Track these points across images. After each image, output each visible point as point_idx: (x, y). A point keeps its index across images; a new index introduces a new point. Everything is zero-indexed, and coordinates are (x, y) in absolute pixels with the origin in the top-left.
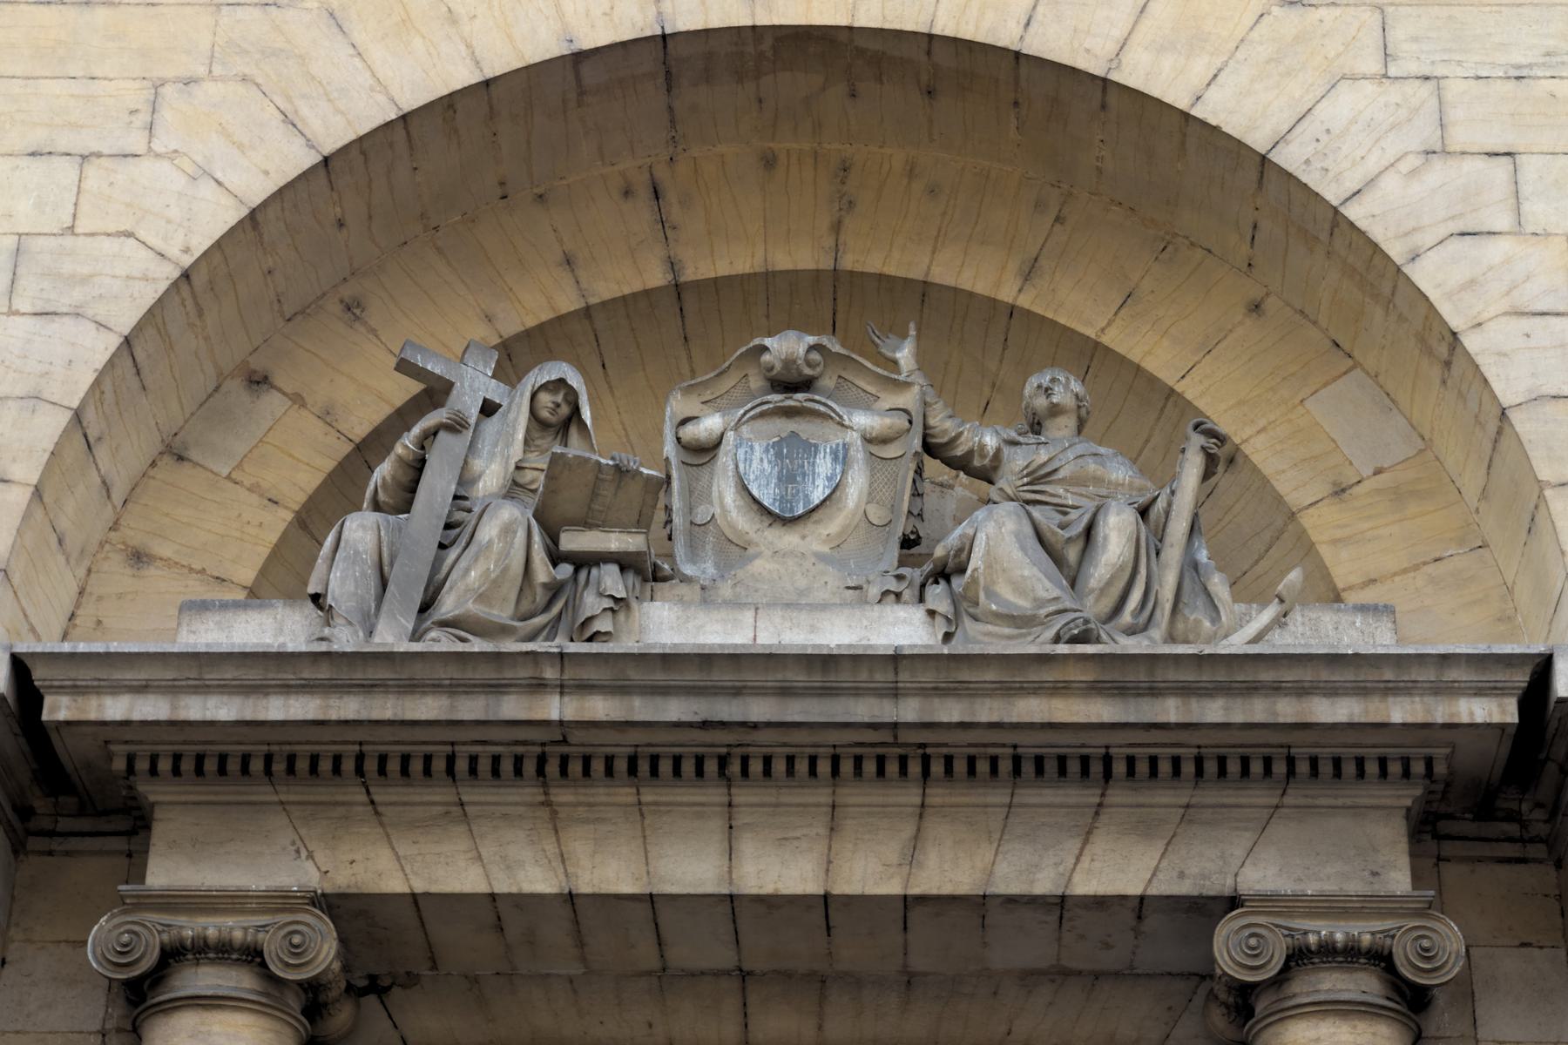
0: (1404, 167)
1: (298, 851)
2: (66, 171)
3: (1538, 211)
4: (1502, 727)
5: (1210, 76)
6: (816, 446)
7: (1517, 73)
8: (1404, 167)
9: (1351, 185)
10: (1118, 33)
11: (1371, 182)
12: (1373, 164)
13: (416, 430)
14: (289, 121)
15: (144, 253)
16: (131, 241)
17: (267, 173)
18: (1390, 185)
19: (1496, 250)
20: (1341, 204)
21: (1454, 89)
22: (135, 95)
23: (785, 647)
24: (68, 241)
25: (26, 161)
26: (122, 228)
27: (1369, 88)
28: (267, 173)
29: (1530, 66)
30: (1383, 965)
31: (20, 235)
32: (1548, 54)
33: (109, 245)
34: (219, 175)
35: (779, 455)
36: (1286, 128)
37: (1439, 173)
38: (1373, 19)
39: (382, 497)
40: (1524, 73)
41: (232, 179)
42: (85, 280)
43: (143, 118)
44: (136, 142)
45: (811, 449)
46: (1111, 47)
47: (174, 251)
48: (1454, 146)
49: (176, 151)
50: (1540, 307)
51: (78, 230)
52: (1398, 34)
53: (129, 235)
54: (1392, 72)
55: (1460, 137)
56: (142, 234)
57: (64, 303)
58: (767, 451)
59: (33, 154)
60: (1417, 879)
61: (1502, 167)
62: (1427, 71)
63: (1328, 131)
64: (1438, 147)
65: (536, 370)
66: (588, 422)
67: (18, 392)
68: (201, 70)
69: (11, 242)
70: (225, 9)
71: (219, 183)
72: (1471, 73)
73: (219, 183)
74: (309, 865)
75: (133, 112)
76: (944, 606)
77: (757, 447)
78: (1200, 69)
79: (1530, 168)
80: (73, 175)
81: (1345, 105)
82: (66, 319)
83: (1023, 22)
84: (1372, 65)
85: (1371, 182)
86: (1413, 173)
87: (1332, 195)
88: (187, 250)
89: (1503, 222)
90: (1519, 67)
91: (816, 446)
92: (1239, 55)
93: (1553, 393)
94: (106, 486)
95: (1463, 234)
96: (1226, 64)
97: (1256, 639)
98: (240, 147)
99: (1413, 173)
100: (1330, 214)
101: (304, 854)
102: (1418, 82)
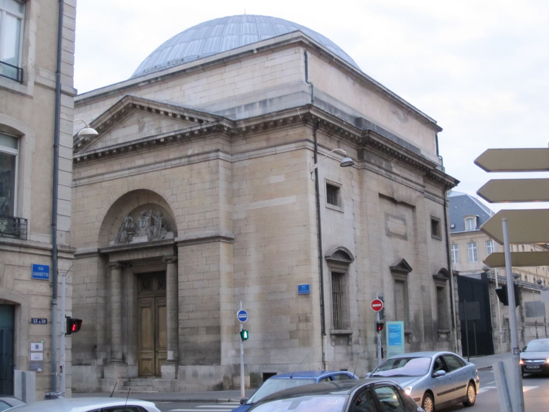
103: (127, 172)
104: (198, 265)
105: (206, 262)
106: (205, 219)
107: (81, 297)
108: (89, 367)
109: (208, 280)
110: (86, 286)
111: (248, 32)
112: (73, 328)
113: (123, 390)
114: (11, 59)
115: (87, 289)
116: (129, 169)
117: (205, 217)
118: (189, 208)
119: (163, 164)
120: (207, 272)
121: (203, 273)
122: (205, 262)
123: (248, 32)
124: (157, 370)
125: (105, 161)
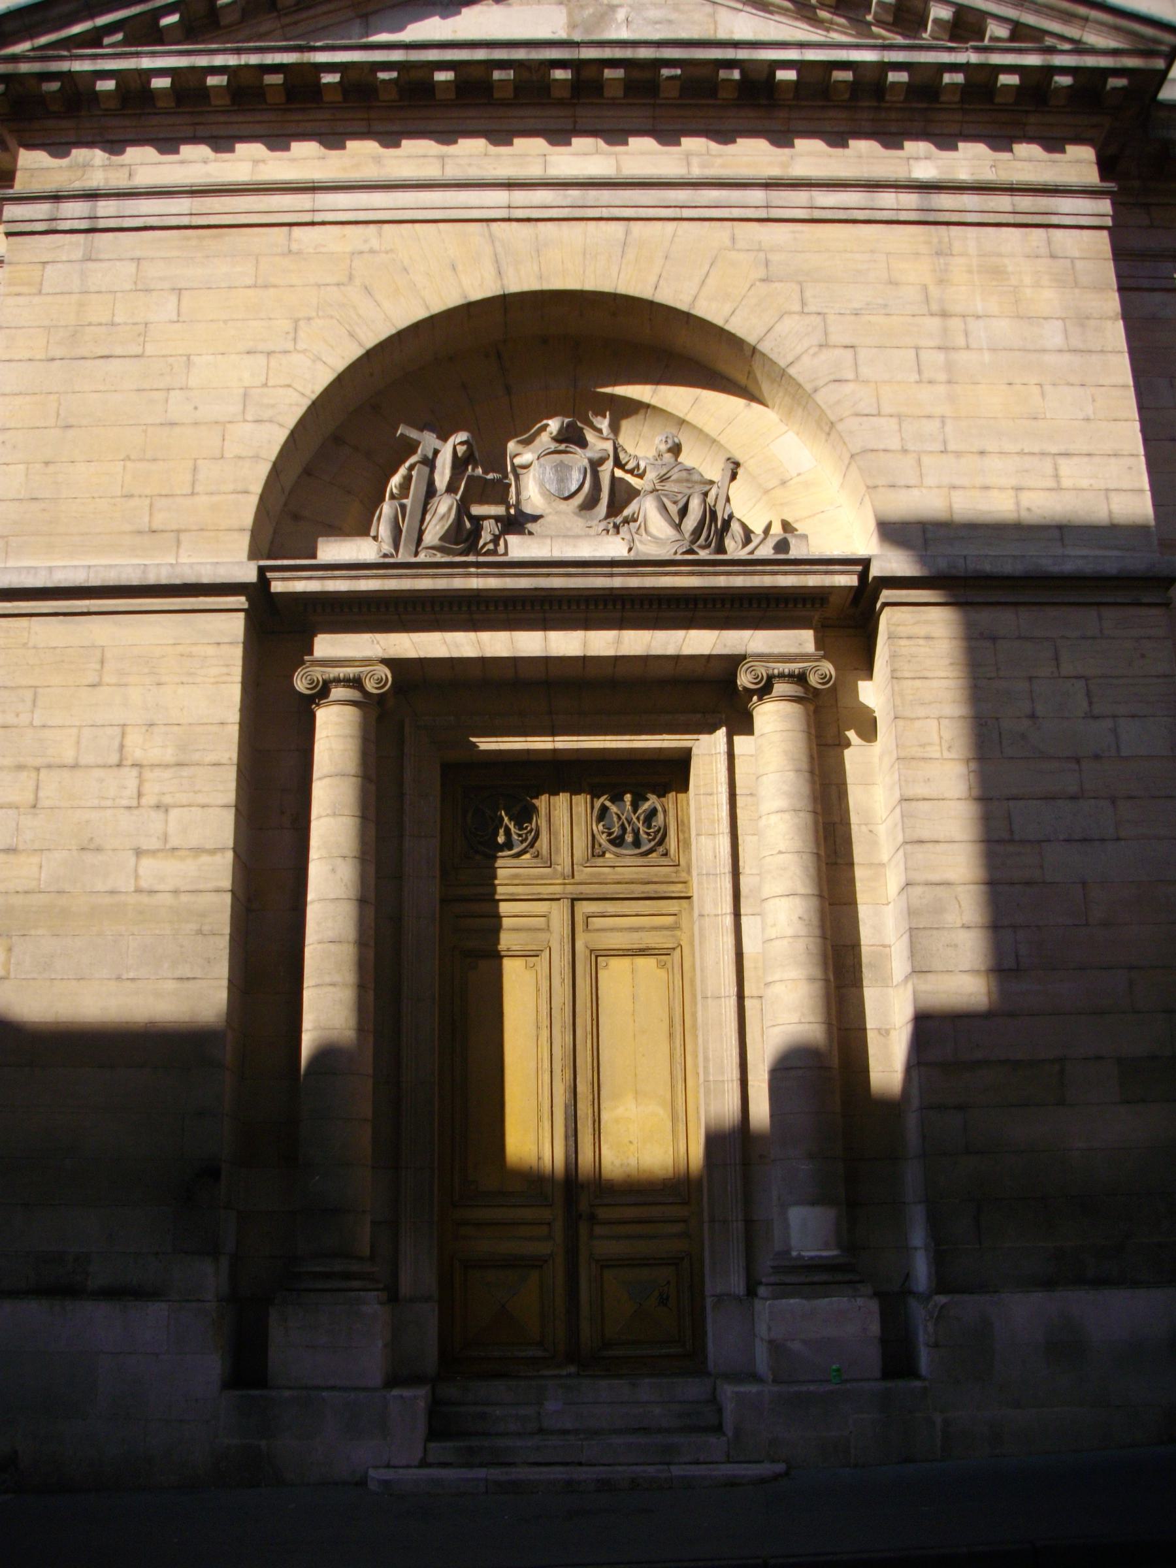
0: (812, 351)
1: (373, 641)
2: (261, 360)
3: (865, 371)
4: (851, 588)
5: (731, 312)
6: (571, 467)
7: (855, 312)
8: (812, 351)
9: (790, 359)
10: (693, 292)
11: (798, 358)
12: (799, 349)
13: (407, 464)
14: (352, 335)
15: (296, 394)
16: (290, 389)
17: (343, 358)
18: (806, 359)
19: (848, 388)
20: (788, 366)
21: (831, 318)
22: (287, 325)
23: (797, 844)
24: (265, 390)
25: (245, 356)
26: (286, 383)
27: (796, 317)
28: (343, 358)
29: (861, 309)
30: (755, 698)
31: (245, 387)
32: (868, 304)
33: (281, 391)
34: (324, 359)
35: (557, 471)
36: (763, 335)
37: (825, 355)
38: (797, 288)
39: (395, 491)
40: (859, 312)
41: (330, 361)
42: (273, 406)
43: (292, 335)
44: (289, 346)
45: (570, 468)
46: (690, 298)
47: (308, 392)
48: (831, 343)
49: (306, 350)
50: (866, 412)
51: (270, 384)
52: (808, 294)
53: (289, 386)
54: (806, 310)
55: (834, 339)
56: (295, 385)
57: (266, 416)
58: (551, 469)
59: (248, 353)
60: (817, 648)
61: (849, 352)
62: (819, 310)
63: (780, 336)
64: (824, 344)
65: (455, 435)
66: (477, 457)
67: (250, 455)
68: (314, 314)
69: (241, 391)
70: (322, 288)
71: (324, 363)
72: (837, 312)
73: (324, 363)
74: (378, 646)
75: (287, 333)
76: (628, 537)
77: (547, 468)
78: (727, 309)
79: (863, 354)
80: (265, 361)
81: (789, 325)
82: (267, 424)
83: (654, 287)
84: (797, 307)
85: (798, 358)
86: (815, 355)
87: (782, 364)
88: (313, 392)
89: (850, 375)
90: (855, 309)
91: (571, 467)
92: (743, 303)
93: (871, 448)
94: (283, 489)
95: (835, 381)
96: (738, 307)
97: (752, 553)
98: (332, 347)
99: (815, 355)
100: (782, 371)
101: (375, 642)
102: (815, 316)
103: (500, 197)
104: (1033, 716)
105: (1090, 703)
106: (1059, 489)
107: (89, 847)
108: (157, 1310)
109: (1113, 800)
110: (141, 781)
111: (723, 875)
112: (497, 834)
113: (470, 1465)
114: (164, 88)
115: (149, 799)
116: (510, 185)
117: (1057, 476)
118: (943, 423)
119: (757, 196)
120: (1097, 757)
121: (1078, 761)
122: (1085, 704)
123: (723, 875)
124: (835, 27)
125: (813, 732)
